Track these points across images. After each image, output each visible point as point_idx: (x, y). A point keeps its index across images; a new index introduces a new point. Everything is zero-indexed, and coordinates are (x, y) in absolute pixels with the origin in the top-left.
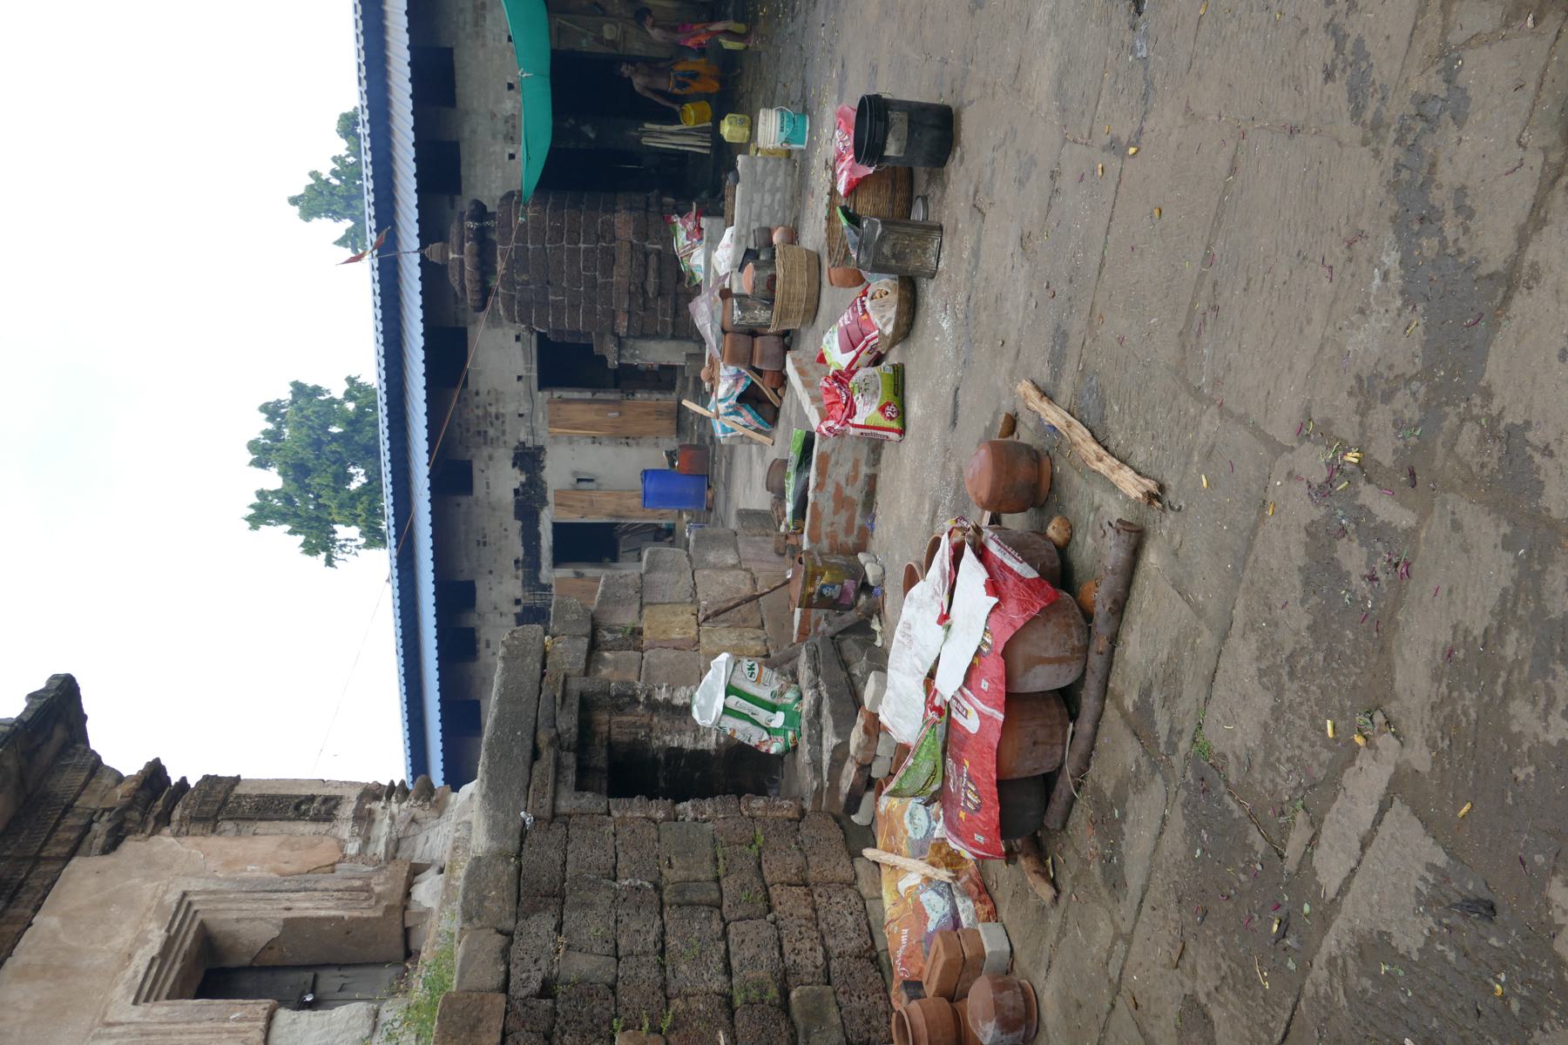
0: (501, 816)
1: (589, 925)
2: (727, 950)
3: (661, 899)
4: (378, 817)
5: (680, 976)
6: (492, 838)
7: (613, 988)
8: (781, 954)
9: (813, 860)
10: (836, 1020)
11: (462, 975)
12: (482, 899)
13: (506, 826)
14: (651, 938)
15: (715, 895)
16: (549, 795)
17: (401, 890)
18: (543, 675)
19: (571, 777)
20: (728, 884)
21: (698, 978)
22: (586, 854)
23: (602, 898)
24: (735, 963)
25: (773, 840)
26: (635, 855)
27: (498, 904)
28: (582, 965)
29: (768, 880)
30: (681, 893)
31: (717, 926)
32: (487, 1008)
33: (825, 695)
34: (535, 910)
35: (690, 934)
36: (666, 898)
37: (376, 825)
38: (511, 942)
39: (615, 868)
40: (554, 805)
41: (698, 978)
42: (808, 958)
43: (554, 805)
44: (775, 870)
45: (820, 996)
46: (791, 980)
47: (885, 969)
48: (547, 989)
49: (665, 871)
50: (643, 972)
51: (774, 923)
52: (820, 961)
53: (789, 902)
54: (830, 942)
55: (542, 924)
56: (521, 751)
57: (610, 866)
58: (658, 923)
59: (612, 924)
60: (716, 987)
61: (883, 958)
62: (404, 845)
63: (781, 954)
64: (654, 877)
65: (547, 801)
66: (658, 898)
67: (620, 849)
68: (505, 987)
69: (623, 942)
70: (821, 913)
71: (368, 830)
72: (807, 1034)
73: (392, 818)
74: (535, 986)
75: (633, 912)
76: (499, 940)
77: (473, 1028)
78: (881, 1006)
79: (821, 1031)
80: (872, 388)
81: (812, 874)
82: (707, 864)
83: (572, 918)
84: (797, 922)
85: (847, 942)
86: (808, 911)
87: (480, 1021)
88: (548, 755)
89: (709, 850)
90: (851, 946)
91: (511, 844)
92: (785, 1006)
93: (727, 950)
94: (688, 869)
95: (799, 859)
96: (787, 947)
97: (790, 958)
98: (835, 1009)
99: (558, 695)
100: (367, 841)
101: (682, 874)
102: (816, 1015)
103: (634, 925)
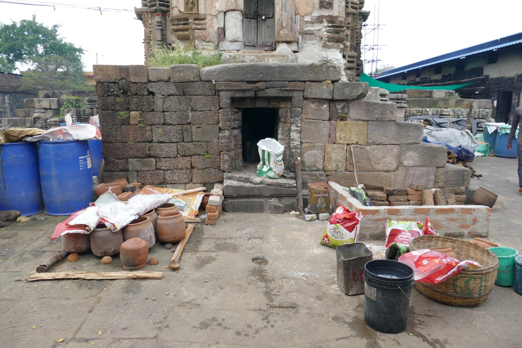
0: (215, 74)
1: (172, 103)
2: (166, 143)
3: (184, 125)
4: (322, 25)
5: (157, 129)
6: (207, 72)
7: (153, 110)
8: (165, 157)
9: (200, 172)
10: (143, 169)
11: (152, 69)
12: (180, 72)
13: (211, 76)
14: (169, 121)
15: (185, 140)
16: (225, 88)
17: (281, 40)
18: (305, 82)
19: (237, 95)
20: (190, 145)
21: (158, 133)
22: (200, 102)
23: (183, 107)
24: (162, 144)
25: (208, 160)
26: (202, 116)
27: (177, 77)
28: (159, 102)
29: (193, 157)
30: (186, 130)
31: (174, 140)
32: (142, 78)
33: (256, 186)
34: (177, 88)
35: (173, 133)
36: (184, 126)
37: (319, 24)
38: (166, 82)
39: (196, 110)
40: (222, 90)
41: (158, 133)
42: (164, 164)
43: (222, 90)
44: (197, 161)
45: (151, 166)
46: (158, 159)
47: (161, 185)
48: (152, 93)
49: (195, 126)
50: (157, 119)
51: (177, 156)
52: (163, 168)
53: (184, 162)
54: (169, 172)
55: (172, 90)
56: (250, 77)
57: (197, 109)
58: (175, 123)
59: (174, 110)
60: (154, 139)
61: (163, 185)
62: (312, 36)
63: (165, 157)
64: (192, 122)
65: (223, 87)
66: (184, 124)
67: (204, 112)
68: (150, 81)
69: (168, 113)
70: (180, 171)
71: (316, 22)
72: (140, 161)
73: (320, 30)
74: (151, 90)
75: (178, 116)
76: (166, 78)
77: (136, 74)
78: (148, 182)
79: (140, 165)
80: (335, 235)
81: (195, 171)
82: (198, 139)
83: (175, 98)
84: (176, 163)
85: (168, 176)
86: (180, 167)
87: (138, 76)
88: (250, 86)
89: (205, 140)
90: (167, 177)
91: (204, 78)
92: (150, 156)
93: (166, 143)
94: (196, 133)
95: (200, 167)
96: (167, 159)
97: (163, 160)
98: (147, 169)
99: (288, 88)
100: (312, 23)
101: (194, 131)
102: (145, 164)
103: (174, 117)
